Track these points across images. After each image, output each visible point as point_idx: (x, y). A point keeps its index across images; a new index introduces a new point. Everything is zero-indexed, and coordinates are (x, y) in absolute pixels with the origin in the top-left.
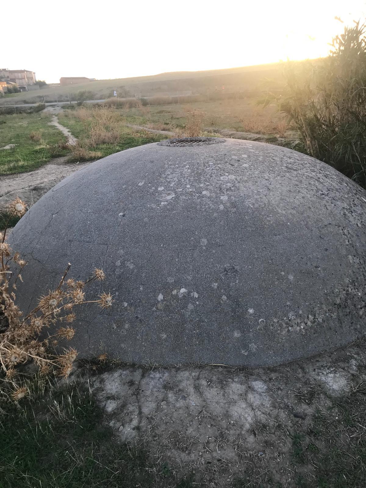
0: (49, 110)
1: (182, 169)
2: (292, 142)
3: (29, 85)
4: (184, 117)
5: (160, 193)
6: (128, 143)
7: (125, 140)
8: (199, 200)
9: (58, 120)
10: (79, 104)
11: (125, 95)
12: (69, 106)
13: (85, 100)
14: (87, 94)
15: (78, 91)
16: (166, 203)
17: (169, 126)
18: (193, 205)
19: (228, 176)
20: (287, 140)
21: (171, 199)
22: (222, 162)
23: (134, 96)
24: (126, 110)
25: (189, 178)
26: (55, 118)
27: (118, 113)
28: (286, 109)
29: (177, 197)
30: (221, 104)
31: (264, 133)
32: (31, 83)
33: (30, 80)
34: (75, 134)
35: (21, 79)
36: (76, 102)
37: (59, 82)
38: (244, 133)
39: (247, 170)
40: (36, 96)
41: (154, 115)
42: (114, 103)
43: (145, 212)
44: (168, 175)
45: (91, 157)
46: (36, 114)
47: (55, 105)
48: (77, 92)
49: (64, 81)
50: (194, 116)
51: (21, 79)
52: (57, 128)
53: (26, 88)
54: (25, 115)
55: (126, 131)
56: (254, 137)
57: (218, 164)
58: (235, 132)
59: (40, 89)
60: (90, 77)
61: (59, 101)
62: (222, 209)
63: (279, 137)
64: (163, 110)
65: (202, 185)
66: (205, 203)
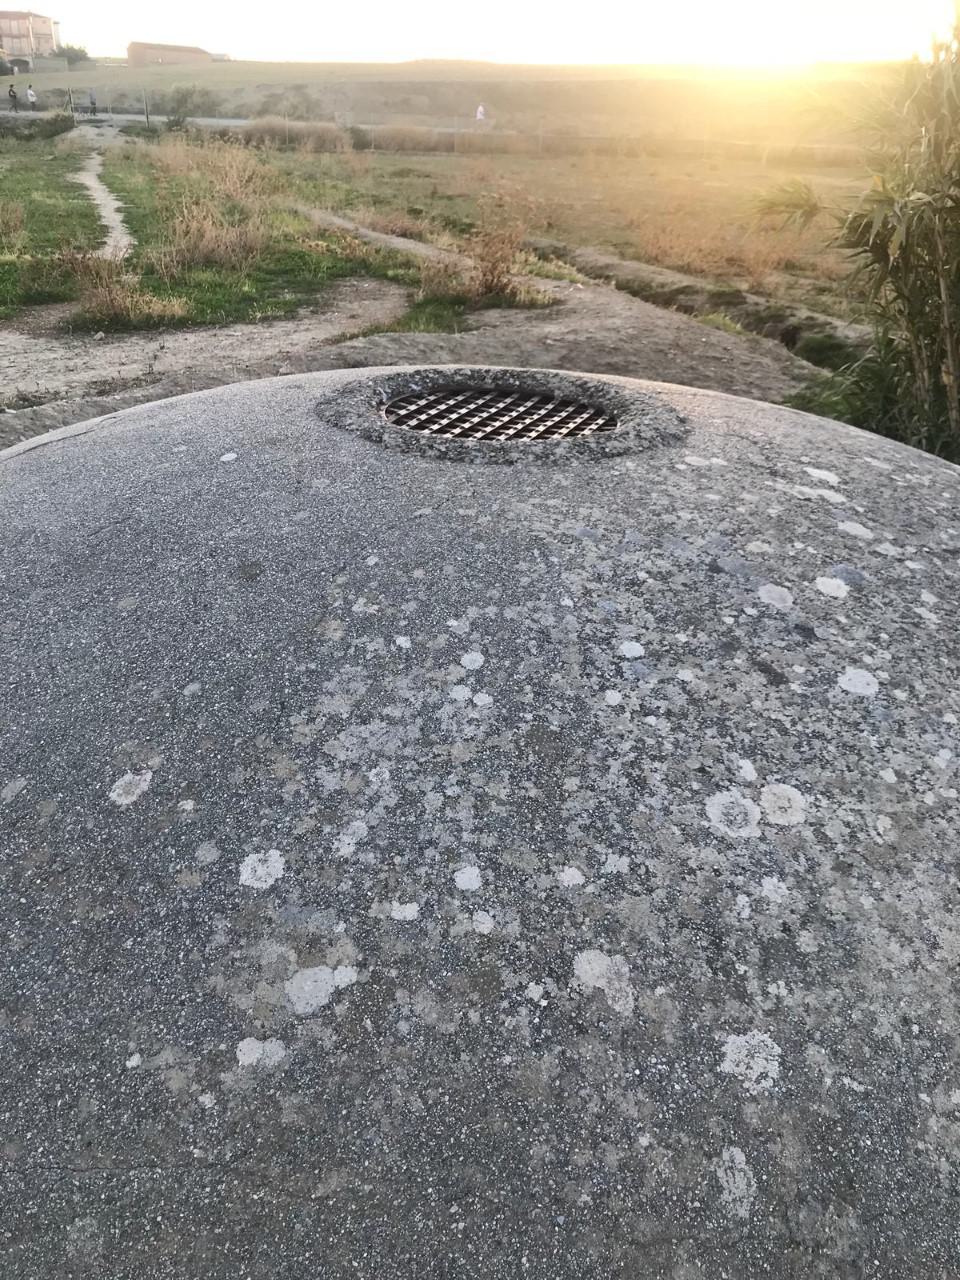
0: (83, 133)
1: (439, 674)
2: (788, 312)
3: (38, 56)
4: (468, 196)
5: (250, 916)
6: (286, 272)
7: (279, 260)
8: (548, 1061)
9: (100, 169)
10: (171, 126)
11: (307, 112)
12: (144, 129)
13: (192, 114)
14: (197, 99)
15: (173, 87)
16: (275, 1052)
17: (423, 224)
18: (498, 1123)
19: (754, 789)
20: (772, 302)
21: (325, 1014)
22: (702, 636)
23: (332, 119)
24: (304, 157)
25: (476, 778)
26: (95, 162)
27: (277, 163)
28: (861, 234)
29: (369, 999)
30: (574, 166)
31: (701, 273)
32: (46, 50)
33: (42, 41)
34: (134, 222)
35: (18, 37)
36: (164, 119)
37: (123, 54)
38: (644, 266)
39: (875, 731)
40: (51, 89)
41: (386, 180)
42: (273, 133)
43: (91, 1132)
44: (336, 723)
45: (149, 316)
46: (43, 143)
47: (102, 121)
48: (170, 88)
49: (141, 53)
50: (500, 206)
51: (18, 37)
52: (88, 193)
53: (31, 65)
54: (12, 141)
55: (292, 227)
56: (673, 283)
57: (678, 660)
58: (615, 260)
59: (70, 70)
60: (214, 48)
61: (115, 111)
62: (743, 1212)
63: (747, 292)
64: (410, 167)
65: (571, 876)
66: (594, 1107)
